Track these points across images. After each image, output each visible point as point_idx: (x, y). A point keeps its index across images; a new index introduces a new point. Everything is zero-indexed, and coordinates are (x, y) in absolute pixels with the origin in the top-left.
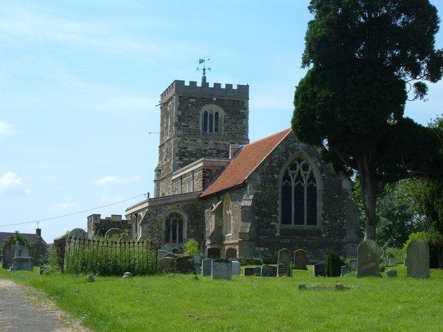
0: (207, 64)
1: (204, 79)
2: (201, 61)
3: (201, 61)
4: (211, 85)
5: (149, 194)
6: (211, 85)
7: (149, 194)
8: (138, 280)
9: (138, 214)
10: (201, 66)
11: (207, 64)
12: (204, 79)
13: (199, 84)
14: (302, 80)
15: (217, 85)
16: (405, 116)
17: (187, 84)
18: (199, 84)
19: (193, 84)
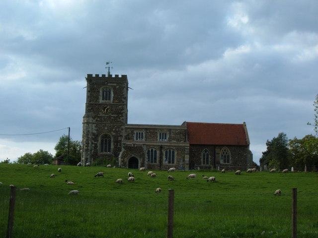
0: (110, 65)
1: (109, 73)
2: (107, 63)
3: (107, 63)
4: (113, 76)
5: (295, 190)
6: (113, 76)
7: (295, 190)
8: (199, 144)
9: (217, 150)
10: (108, 66)
11: (110, 65)
12: (109, 73)
13: (107, 76)
14: (86, 103)
15: (97, 76)
16: (132, 120)
17: (94, 76)
18: (107, 76)
19: (104, 76)
